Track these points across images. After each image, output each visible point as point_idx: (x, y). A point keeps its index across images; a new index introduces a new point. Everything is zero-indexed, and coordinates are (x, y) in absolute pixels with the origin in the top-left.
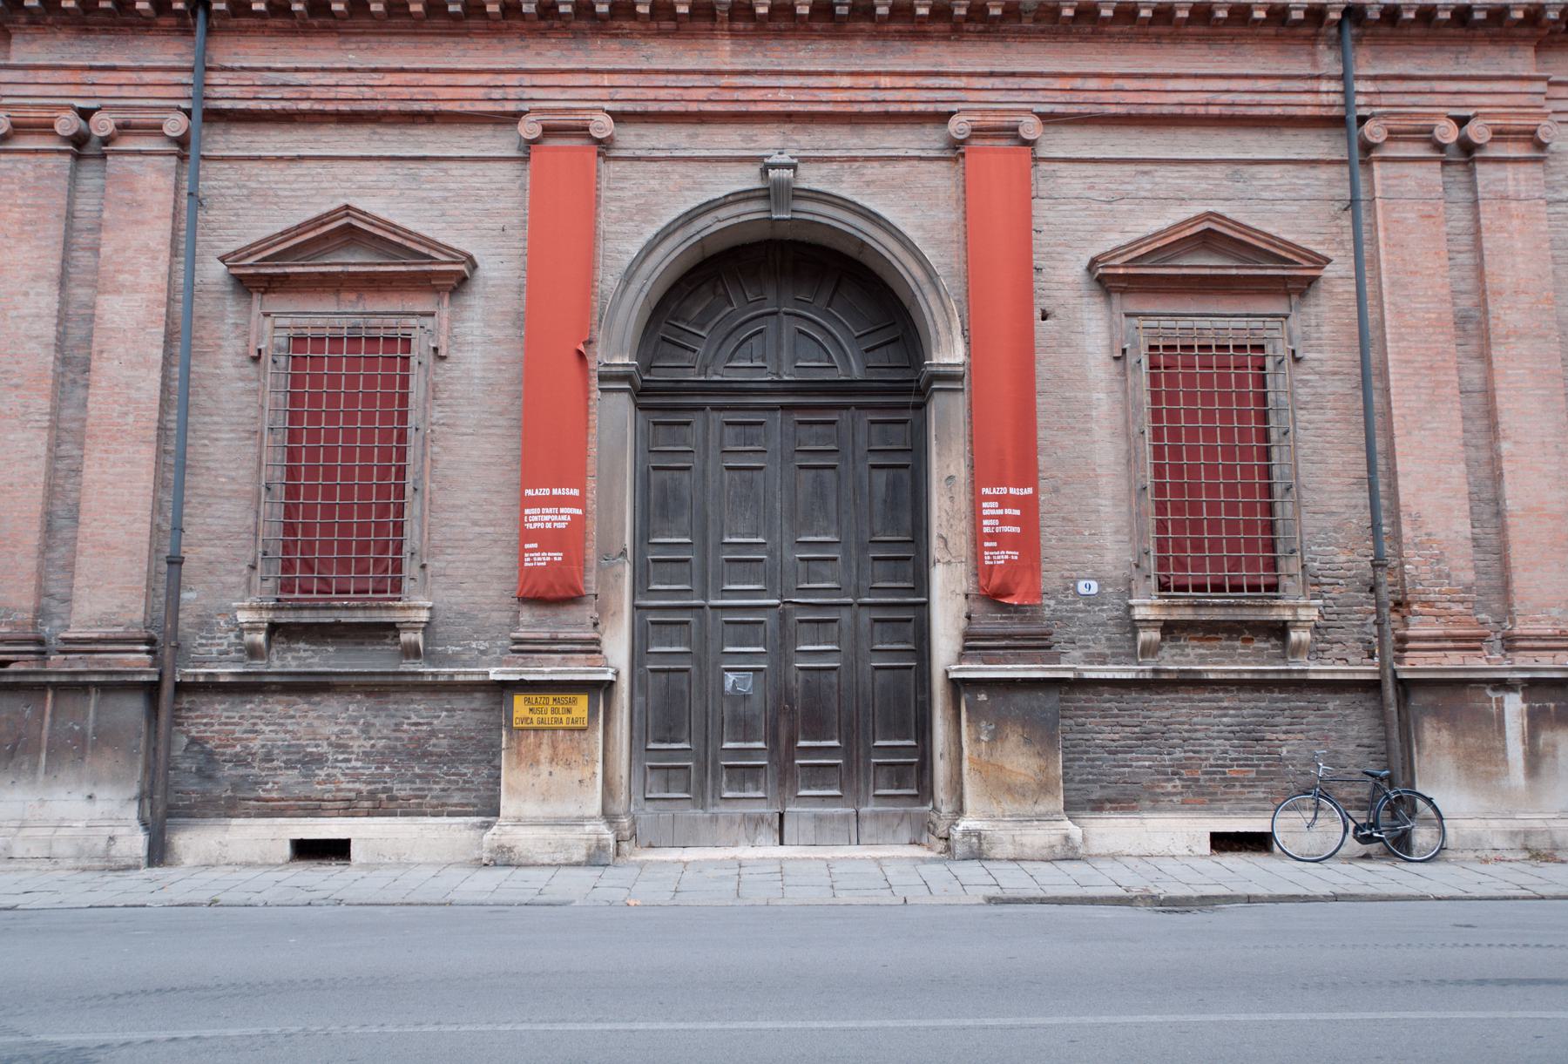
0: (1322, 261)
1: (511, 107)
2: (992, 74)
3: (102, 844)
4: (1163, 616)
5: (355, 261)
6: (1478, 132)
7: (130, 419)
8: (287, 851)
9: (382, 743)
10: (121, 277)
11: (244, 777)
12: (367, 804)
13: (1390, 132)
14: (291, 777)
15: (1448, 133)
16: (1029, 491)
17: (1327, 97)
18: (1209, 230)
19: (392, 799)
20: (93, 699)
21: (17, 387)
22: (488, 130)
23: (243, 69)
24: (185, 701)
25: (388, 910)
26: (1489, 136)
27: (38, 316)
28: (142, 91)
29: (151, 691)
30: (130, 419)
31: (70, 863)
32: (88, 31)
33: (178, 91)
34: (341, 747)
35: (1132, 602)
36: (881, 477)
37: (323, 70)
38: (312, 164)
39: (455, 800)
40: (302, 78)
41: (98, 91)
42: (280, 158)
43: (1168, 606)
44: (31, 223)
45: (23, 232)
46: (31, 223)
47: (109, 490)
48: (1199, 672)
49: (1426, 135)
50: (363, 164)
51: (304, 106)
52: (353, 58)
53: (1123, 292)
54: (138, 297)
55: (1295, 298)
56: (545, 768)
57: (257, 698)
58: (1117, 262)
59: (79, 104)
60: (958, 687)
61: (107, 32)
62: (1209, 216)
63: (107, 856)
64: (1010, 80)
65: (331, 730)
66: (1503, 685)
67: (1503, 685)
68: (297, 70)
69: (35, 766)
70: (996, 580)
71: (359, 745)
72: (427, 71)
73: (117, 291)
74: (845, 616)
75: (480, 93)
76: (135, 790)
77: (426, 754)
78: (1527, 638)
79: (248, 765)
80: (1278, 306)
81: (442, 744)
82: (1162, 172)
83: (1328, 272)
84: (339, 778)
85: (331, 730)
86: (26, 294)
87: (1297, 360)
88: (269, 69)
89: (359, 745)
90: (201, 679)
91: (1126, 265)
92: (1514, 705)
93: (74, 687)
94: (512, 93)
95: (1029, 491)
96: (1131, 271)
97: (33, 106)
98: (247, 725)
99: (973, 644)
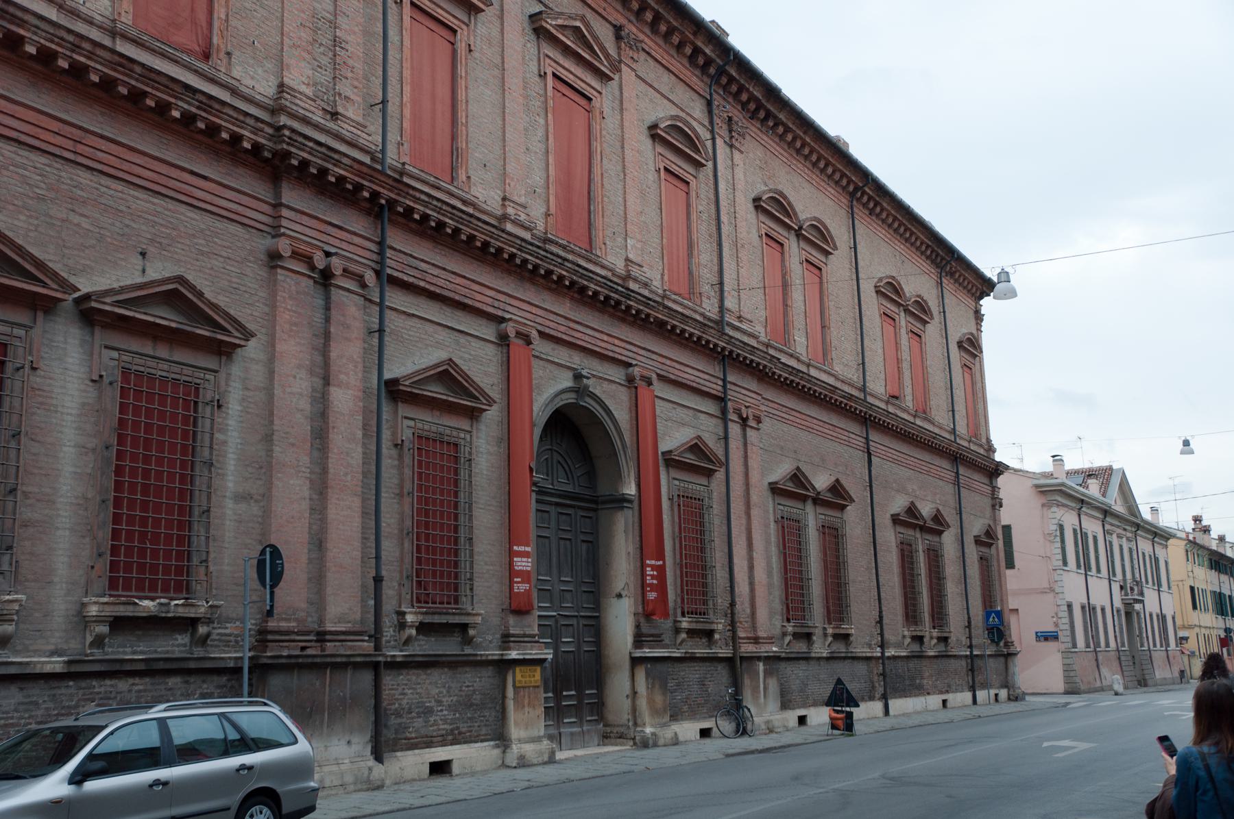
0: (248, 335)
1: (500, 313)
2: (644, 349)
3: (366, 773)
4: (111, 611)
5: (166, 317)
6: (337, 264)
7: (349, 478)
8: (427, 769)
9: (455, 699)
10: (342, 376)
11: (400, 724)
12: (450, 737)
13: (293, 252)
14: (419, 723)
15: (320, 261)
16: (660, 563)
17: (715, 388)
18: (176, 289)
19: (460, 733)
20: (349, 672)
21: (293, 445)
22: (484, 322)
23: (400, 251)
24: (745, 665)
25: (425, 810)
26: (289, 254)
27: (301, 394)
28: (351, 248)
29: (729, 661)
30: (349, 478)
31: (352, 787)
32: (322, 193)
33: (368, 254)
34: (439, 702)
35: (85, 600)
36: (584, 546)
37: (433, 265)
38: (417, 320)
39: (483, 732)
40: (423, 266)
41: (332, 240)
42: (404, 313)
43: (426, 613)
44: (296, 324)
45: (291, 330)
46: (296, 324)
47: (341, 527)
48: (28, 663)
49: (308, 260)
50: (440, 328)
51: (422, 284)
52: (439, 260)
53: (105, 326)
54: (350, 392)
55: (40, 315)
56: (526, 709)
57: (404, 672)
58: (108, 300)
59: (327, 248)
60: (635, 662)
61: (331, 198)
62: (181, 280)
63: (368, 781)
64: (113, 146)
65: (435, 691)
66: (759, 658)
67: (759, 658)
68: (422, 260)
69: (322, 722)
70: (651, 607)
71: (446, 700)
72: (473, 281)
73: (339, 386)
74: (574, 622)
75: (489, 301)
76: (368, 737)
77: (472, 705)
78: (331, 633)
79: (401, 716)
80: (22, 317)
81: (477, 698)
82: (679, 409)
83: (252, 343)
84: (440, 721)
85: (435, 691)
86: (295, 377)
87: (34, 369)
88: (411, 256)
89: (446, 700)
90: (399, 659)
91: (119, 303)
92: (761, 666)
93: (343, 666)
94: (502, 306)
95: (660, 563)
96: (117, 310)
97: (305, 242)
98: (400, 690)
99: (639, 641)
